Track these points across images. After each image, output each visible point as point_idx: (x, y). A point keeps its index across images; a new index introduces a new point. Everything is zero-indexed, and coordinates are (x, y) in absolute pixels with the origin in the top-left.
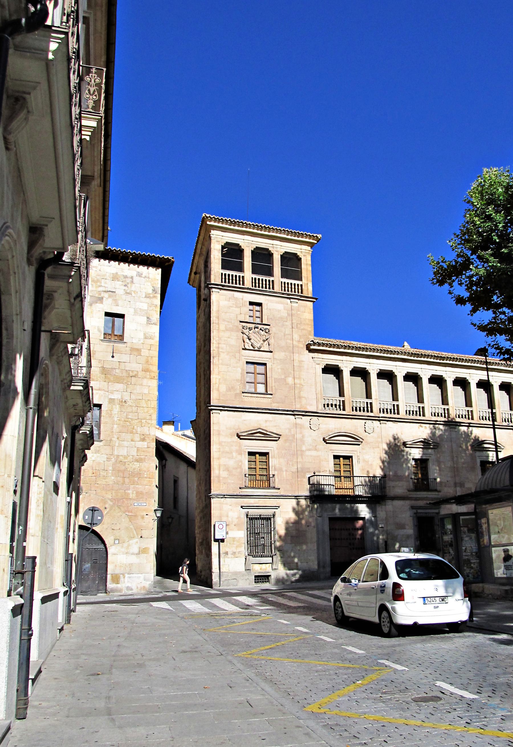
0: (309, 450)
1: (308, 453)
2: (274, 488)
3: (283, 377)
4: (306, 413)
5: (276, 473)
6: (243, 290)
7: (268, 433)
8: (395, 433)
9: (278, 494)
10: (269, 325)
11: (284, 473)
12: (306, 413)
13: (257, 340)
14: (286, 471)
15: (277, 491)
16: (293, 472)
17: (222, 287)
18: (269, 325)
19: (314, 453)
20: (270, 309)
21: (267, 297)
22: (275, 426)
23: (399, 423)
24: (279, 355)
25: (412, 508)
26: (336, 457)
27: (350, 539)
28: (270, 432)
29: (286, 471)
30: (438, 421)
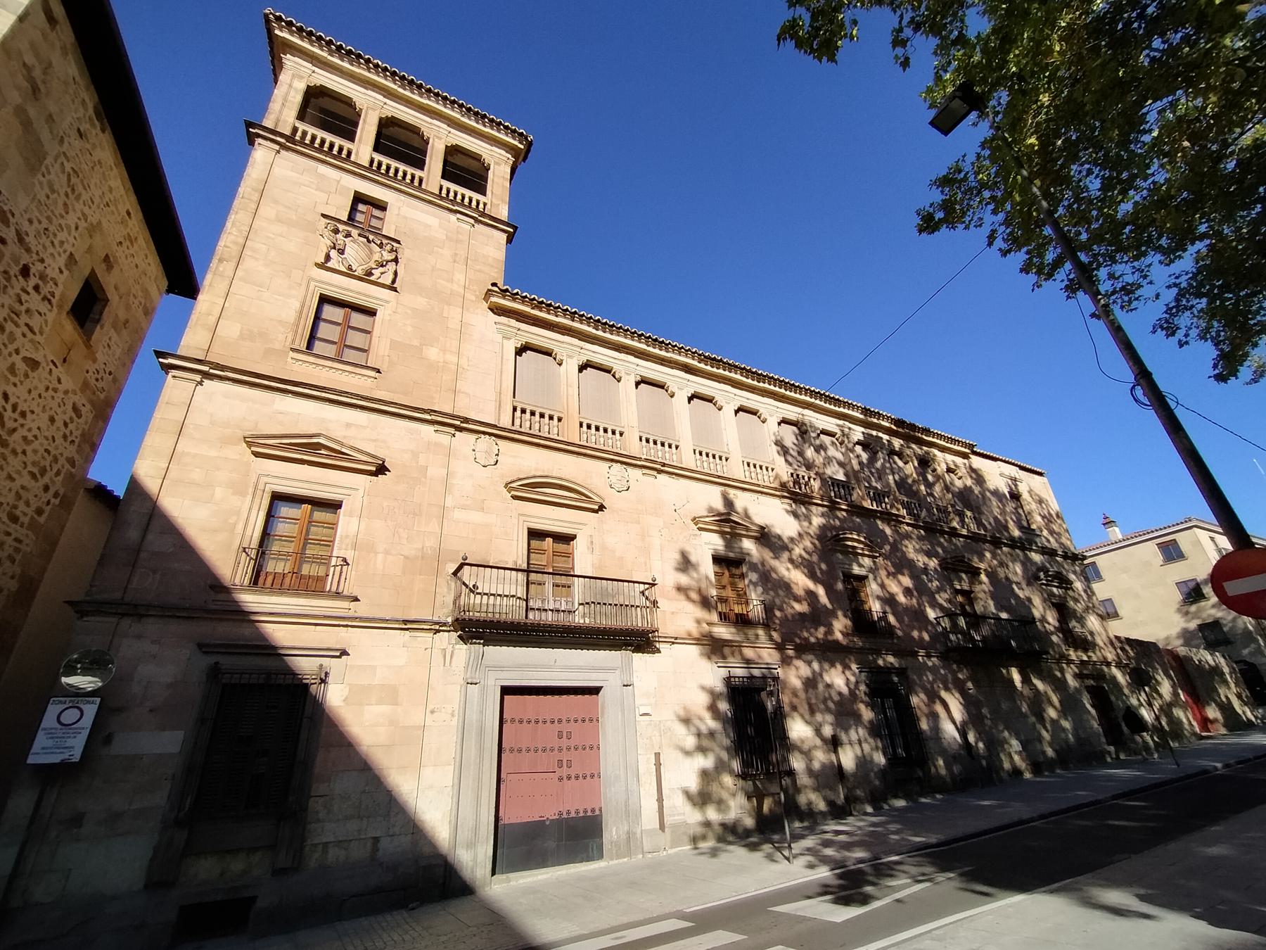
0: (464, 507)
1: (458, 514)
2: (338, 595)
3: (416, 343)
4: (461, 425)
5: (349, 555)
6: (342, 159)
7: (344, 450)
8: (994, 251)
9: (351, 613)
10: (398, 242)
11: (380, 557)
12: (461, 425)
13: (356, 253)
14: (387, 552)
15: (345, 604)
16: (406, 557)
17: (290, 142)
18: (398, 242)
19: (476, 517)
20: (405, 218)
21: (402, 197)
22: (374, 441)
23: (682, 480)
24: (408, 299)
25: (204, 648)
26: (534, 534)
27: (560, 750)
28: (352, 448)
29: (387, 552)
30: (878, 415)
